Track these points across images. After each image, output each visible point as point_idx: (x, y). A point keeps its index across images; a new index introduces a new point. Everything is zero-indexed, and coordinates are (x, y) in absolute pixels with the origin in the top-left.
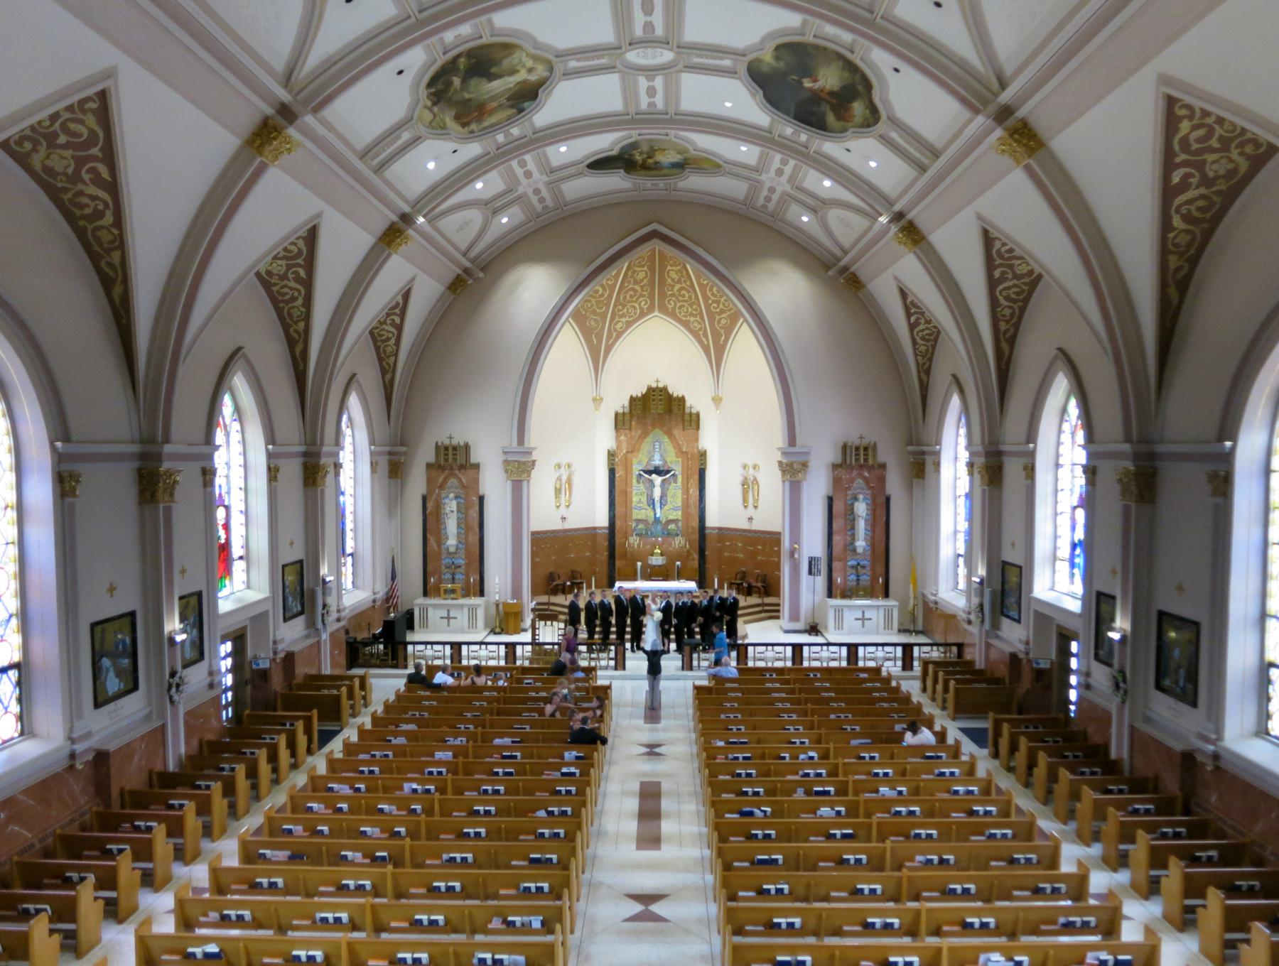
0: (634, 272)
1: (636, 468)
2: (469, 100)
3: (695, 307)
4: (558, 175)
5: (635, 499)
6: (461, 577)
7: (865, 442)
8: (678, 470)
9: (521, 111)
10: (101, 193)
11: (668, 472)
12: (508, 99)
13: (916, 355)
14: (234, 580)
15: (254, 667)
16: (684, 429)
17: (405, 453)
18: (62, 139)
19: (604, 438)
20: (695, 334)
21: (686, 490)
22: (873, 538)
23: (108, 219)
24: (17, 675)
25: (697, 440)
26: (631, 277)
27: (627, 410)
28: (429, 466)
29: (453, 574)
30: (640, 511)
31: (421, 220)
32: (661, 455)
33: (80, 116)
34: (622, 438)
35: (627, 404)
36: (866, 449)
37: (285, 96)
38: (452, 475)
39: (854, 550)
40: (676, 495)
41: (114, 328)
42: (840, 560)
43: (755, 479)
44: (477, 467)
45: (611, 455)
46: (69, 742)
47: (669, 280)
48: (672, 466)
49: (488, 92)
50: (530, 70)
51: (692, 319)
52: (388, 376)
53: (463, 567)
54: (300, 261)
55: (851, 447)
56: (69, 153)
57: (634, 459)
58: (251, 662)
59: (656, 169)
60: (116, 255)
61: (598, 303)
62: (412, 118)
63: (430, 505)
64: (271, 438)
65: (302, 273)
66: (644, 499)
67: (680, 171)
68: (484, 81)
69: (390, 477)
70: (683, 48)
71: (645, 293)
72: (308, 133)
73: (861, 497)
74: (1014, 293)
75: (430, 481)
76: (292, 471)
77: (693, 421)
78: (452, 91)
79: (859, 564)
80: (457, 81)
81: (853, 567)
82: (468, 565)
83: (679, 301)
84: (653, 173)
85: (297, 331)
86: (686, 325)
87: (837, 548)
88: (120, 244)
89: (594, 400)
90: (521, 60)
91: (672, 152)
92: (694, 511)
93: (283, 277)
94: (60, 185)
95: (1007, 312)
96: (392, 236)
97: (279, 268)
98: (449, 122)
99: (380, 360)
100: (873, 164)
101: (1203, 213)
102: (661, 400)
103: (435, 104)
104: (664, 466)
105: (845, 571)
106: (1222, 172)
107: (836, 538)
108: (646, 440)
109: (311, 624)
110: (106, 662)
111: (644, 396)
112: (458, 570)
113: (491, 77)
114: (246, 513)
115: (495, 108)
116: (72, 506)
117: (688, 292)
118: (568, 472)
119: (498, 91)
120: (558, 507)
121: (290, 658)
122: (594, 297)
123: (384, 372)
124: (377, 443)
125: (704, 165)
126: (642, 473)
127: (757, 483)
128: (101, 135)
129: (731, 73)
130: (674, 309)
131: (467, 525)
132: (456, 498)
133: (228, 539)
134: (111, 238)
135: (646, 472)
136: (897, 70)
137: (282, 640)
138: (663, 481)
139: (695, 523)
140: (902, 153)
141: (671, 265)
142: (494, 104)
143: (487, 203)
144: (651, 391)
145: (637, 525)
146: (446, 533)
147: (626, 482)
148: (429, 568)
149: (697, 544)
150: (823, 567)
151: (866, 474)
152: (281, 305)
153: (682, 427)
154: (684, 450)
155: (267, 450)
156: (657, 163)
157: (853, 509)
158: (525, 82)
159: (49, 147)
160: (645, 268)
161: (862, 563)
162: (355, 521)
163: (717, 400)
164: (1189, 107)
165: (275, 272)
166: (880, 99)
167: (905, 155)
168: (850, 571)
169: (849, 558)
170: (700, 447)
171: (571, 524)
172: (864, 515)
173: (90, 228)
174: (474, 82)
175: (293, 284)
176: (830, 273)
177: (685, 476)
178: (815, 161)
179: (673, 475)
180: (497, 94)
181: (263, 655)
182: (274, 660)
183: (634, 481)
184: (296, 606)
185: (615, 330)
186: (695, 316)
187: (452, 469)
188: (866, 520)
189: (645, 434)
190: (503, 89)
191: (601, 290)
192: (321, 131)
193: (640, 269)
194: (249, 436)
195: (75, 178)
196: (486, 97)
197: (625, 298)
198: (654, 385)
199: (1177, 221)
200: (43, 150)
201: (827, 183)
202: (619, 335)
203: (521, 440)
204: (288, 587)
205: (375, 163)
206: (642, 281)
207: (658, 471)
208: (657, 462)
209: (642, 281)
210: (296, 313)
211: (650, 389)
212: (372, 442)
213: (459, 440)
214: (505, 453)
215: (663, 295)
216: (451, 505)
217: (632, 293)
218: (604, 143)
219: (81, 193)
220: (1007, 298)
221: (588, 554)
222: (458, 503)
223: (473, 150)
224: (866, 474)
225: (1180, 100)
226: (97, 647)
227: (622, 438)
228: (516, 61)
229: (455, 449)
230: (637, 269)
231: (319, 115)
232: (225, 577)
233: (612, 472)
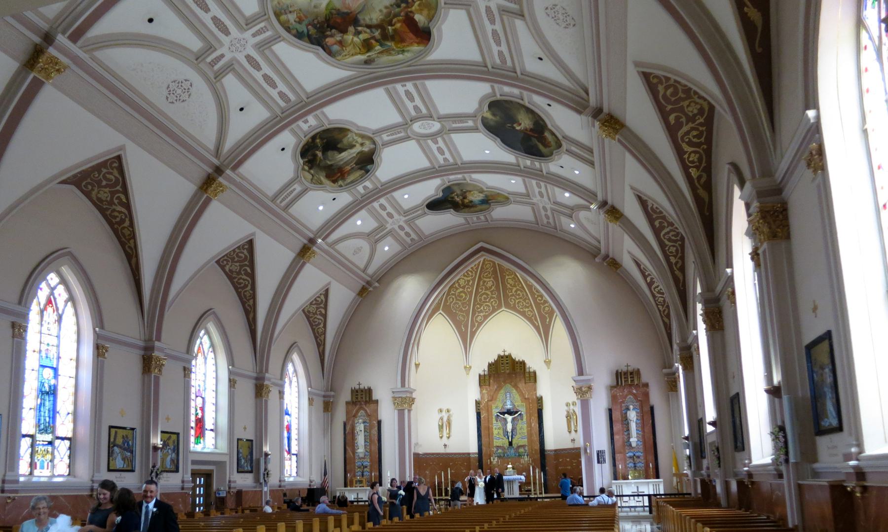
0: (484, 282)
1: (495, 412)
2: (332, 165)
3: (527, 301)
4: (410, 214)
5: (495, 432)
6: (368, 474)
7: (630, 369)
8: (523, 410)
9: (367, 171)
10: (123, 210)
11: (516, 412)
12: (356, 164)
13: (657, 305)
14: (206, 441)
15: (217, 495)
16: (525, 383)
17: (333, 396)
18: (104, 183)
19: (473, 392)
20: (530, 320)
21: (529, 425)
22: (643, 436)
23: (127, 223)
24: (69, 444)
25: (535, 390)
26: (482, 285)
27: (486, 373)
28: (347, 403)
29: (363, 472)
30: (499, 441)
31: (320, 240)
32: (511, 402)
33: (111, 171)
34: (484, 391)
35: (486, 369)
36: (631, 373)
37: (216, 161)
38: (361, 408)
39: (630, 445)
40: (523, 427)
41: (132, 278)
42: (620, 453)
43: (574, 411)
44: (377, 402)
45: (478, 403)
46: (91, 482)
47: (508, 285)
48: (520, 409)
49: (342, 160)
50: (362, 145)
51: (527, 310)
52: (321, 348)
53: (369, 467)
54: (246, 263)
55: (621, 373)
56: (107, 190)
57: (493, 405)
58: (215, 492)
59: (472, 206)
60: (132, 241)
61: (463, 304)
62: (298, 177)
63: (348, 428)
64: (231, 361)
65: (249, 270)
66: (501, 432)
67: (487, 206)
68: (336, 153)
69: (324, 411)
70: (441, 118)
71: (494, 296)
72: (230, 180)
73: (631, 407)
74: (672, 236)
75: (348, 413)
76: (247, 388)
77: (533, 377)
78: (319, 160)
79: (634, 455)
80: (319, 154)
81: (630, 457)
82: (371, 466)
83: (517, 299)
84: (472, 209)
85: (249, 305)
86: (523, 314)
87: (618, 444)
88: (133, 236)
89: (465, 367)
90: (353, 138)
91: (475, 192)
92: (536, 438)
93: (239, 273)
94: (105, 207)
95: (673, 249)
96: (305, 252)
97: (236, 268)
98: (323, 179)
99: (316, 338)
100: (577, 172)
101: (698, 139)
102: (507, 363)
103: (310, 168)
104: (513, 409)
105: (625, 461)
106: (696, 111)
107: (616, 437)
108: (500, 392)
109: (257, 480)
110: (116, 449)
111: (496, 362)
112: (365, 469)
113: (341, 151)
114: (216, 405)
115: (350, 170)
116: (103, 362)
117: (521, 291)
118: (447, 415)
119: (347, 159)
120: (441, 437)
121: (239, 493)
122: (460, 301)
123: (319, 345)
124: (313, 387)
125: (500, 199)
126: (498, 414)
127: (576, 414)
128: (121, 179)
129: (475, 129)
130: (514, 304)
131: (370, 440)
132: (364, 422)
133: (203, 416)
134: (129, 232)
135: (501, 413)
136: (549, 105)
137: (235, 482)
138: (513, 419)
139: (537, 447)
140: (572, 154)
141: (508, 275)
142: (348, 168)
143: (368, 235)
144: (500, 357)
145: (498, 450)
146: (358, 446)
147: (488, 421)
148: (348, 468)
149: (539, 462)
150: (608, 457)
151: (634, 391)
152: (240, 290)
153: (524, 381)
154: (526, 397)
155: (229, 369)
156: (471, 202)
157: (626, 416)
158: (361, 152)
159: (98, 187)
160: (492, 279)
161: (637, 454)
162: (299, 434)
163: (548, 363)
164: (657, 77)
165: (234, 270)
166: (552, 126)
167: (576, 155)
168: (629, 461)
169: (627, 451)
170: (538, 395)
171: (451, 450)
172: (635, 419)
173: (120, 228)
174: (330, 153)
175: (244, 277)
176: (597, 260)
177: (529, 415)
178: (547, 178)
179: (520, 414)
180: (347, 161)
181: (222, 489)
182: (229, 492)
183: (494, 419)
184: (247, 466)
185: (477, 321)
186: (528, 307)
187: (361, 404)
188: (636, 423)
189: (499, 388)
190: (349, 158)
191: (464, 295)
192: (238, 179)
193: (488, 280)
194: (218, 361)
195: (111, 203)
196: (342, 163)
197: (480, 300)
198: (502, 354)
199: (686, 148)
200: (96, 190)
201: (567, 195)
202: (480, 324)
203: (403, 385)
204: (241, 453)
205: (283, 204)
206: (491, 288)
207: (510, 412)
208: (509, 406)
209: (491, 288)
210: (248, 294)
211: (500, 357)
212: (309, 385)
213: (365, 385)
214: (393, 392)
215: (506, 297)
216: (360, 427)
217: (485, 296)
218: (430, 189)
219: (114, 210)
220: (670, 240)
221: (464, 471)
222: (365, 426)
223: (345, 198)
224: (634, 391)
225: (651, 74)
226: (112, 440)
227: (484, 391)
228: (351, 139)
229: (362, 391)
230: (486, 280)
231: (237, 172)
232: (200, 438)
233: (479, 415)
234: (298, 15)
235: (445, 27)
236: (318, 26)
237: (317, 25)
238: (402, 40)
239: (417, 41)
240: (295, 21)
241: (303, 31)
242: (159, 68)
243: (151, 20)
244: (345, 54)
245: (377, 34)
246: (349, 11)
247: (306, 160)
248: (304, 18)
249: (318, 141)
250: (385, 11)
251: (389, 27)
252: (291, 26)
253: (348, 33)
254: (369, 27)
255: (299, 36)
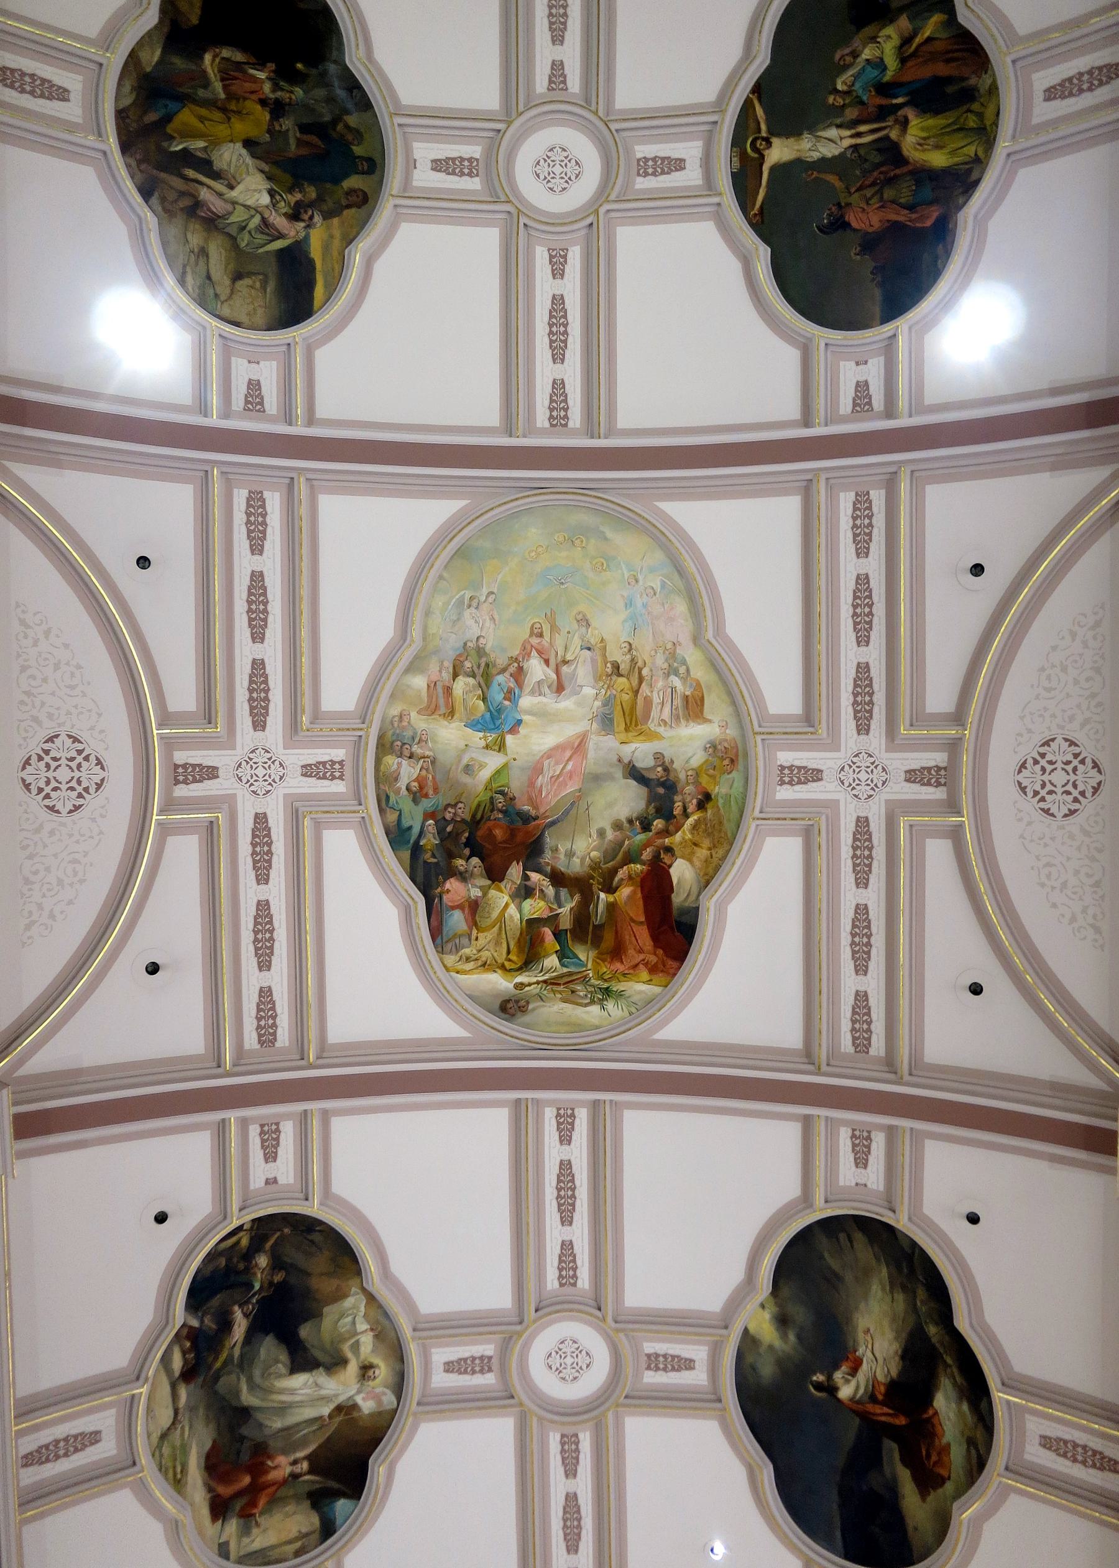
78: (224, 1355)
103: (188, 1375)
158: (346, 1410)
234: (424, 773)
235: (734, 909)
236: (449, 829)
237: (448, 822)
238: (617, 952)
239: (653, 959)
240: (408, 789)
241: (410, 828)
242: (72, 675)
243: (143, 562)
244: (467, 951)
245: (567, 909)
246: (533, 813)
247: (195, 1323)
248: (431, 792)
249: (262, 1261)
250: (610, 835)
251: (602, 895)
252: (392, 799)
253: (502, 885)
254: (558, 879)
255: (397, 836)
